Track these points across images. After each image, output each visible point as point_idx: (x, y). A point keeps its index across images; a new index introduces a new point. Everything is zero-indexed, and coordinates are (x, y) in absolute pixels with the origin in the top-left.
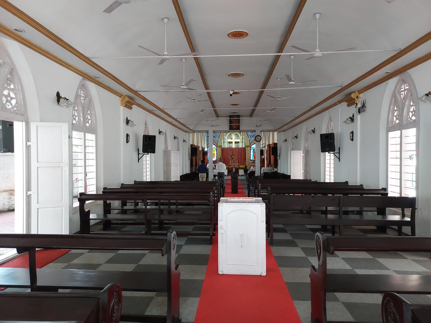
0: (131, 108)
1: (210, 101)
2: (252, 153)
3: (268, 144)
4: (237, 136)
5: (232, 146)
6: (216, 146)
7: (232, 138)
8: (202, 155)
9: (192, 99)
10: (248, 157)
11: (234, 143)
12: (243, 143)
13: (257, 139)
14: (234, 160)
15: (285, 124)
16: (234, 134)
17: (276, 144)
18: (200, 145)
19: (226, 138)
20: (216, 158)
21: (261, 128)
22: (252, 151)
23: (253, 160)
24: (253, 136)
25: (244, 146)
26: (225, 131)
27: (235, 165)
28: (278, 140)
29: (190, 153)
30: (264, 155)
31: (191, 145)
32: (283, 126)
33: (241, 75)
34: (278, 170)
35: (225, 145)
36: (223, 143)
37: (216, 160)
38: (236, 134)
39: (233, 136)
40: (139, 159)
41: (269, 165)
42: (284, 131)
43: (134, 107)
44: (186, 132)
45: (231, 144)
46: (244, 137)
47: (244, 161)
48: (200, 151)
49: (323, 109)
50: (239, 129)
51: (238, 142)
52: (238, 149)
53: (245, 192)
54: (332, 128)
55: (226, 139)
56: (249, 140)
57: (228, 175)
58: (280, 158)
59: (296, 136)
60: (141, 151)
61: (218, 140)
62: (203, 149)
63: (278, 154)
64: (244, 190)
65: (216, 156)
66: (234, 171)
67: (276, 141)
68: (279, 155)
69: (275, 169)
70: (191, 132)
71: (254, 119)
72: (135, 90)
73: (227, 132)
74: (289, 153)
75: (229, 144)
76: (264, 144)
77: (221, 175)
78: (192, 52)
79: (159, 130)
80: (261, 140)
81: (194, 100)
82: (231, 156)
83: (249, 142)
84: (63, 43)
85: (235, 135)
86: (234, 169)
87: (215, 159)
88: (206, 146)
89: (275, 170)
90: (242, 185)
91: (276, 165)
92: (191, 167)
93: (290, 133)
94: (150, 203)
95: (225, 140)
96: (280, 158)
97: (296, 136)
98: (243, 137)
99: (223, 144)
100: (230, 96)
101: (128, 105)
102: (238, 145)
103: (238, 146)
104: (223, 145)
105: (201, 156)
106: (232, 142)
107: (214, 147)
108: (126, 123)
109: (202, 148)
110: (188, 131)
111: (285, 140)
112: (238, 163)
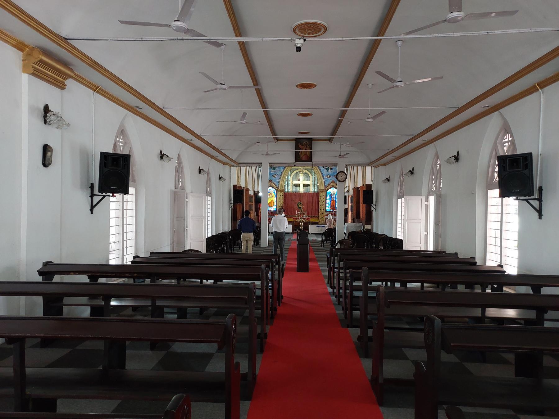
0: (62, 86)
1: (255, 89)
2: (328, 201)
3: (355, 188)
4: (306, 176)
5: (299, 190)
6: (276, 190)
7: (300, 179)
8: (253, 202)
9: (216, 83)
10: (323, 206)
11: (301, 186)
12: (315, 186)
13: (339, 178)
14: (302, 211)
15: (389, 151)
16: (302, 173)
17: (369, 186)
18: (250, 187)
19: (291, 179)
20: (275, 207)
21: (347, 160)
22: (328, 197)
23: (330, 211)
24: (331, 176)
25: (316, 191)
26: (288, 164)
27: (303, 218)
28: (373, 179)
29: (232, 198)
30: (347, 204)
31: (235, 186)
32: (386, 155)
33: (320, 31)
34: (372, 227)
35: (290, 189)
36: (286, 185)
37: (276, 210)
38: (305, 174)
39: (301, 177)
40: (92, 207)
41: (356, 220)
42: (385, 165)
43: (70, 83)
44: (224, 163)
45: (298, 187)
46: (316, 178)
47: (317, 213)
48: (250, 196)
49: (489, 108)
50: (311, 161)
51: (308, 185)
52: (307, 195)
53: (321, 268)
54: (440, 166)
55: (291, 180)
56: (325, 182)
57: (293, 233)
58: (376, 209)
59: (412, 171)
60: (96, 191)
61: (279, 181)
62: (256, 194)
63: (374, 203)
64: (319, 263)
65: (275, 204)
66: (301, 227)
67: (368, 182)
68: (375, 204)
69: (366, 226)
70: (233, 164)
71: (335, 146)
72: (64, 34)
73: (292, 165)
74: (394, 200)
75: (294, 187)
76: (350, 185)
77: (279, 237)
78: (254, 85)
79: (220, 176)
80: (345, 180)
81: (222, 84)
82: (298, 205)
83: (325, 184)
84: (44, 30)
85: (304, 174)
86: (302, 224)
87: (273, 209)
88: (260, 190)
89: (367, 227)
90: (314, 251)
91: (369, 219)
92: (233, 221)
93: (395, 169)
94: (112, 307)
95: (289, 182)
96: (376, 209)
97: (412, 171)
98: (315, 177)
99: (286, 187)
100: (297, 51)
101: (59, 80)
102: (307, 189)
103: (308, 190)
104: (286, 189)
105: (253, 204)
106: (299, 185)
107: (273, 191)
108: (160, 158)
109: (254, 191)
110: (228, 162)
111: (387, 179)
112: (308, 214)
